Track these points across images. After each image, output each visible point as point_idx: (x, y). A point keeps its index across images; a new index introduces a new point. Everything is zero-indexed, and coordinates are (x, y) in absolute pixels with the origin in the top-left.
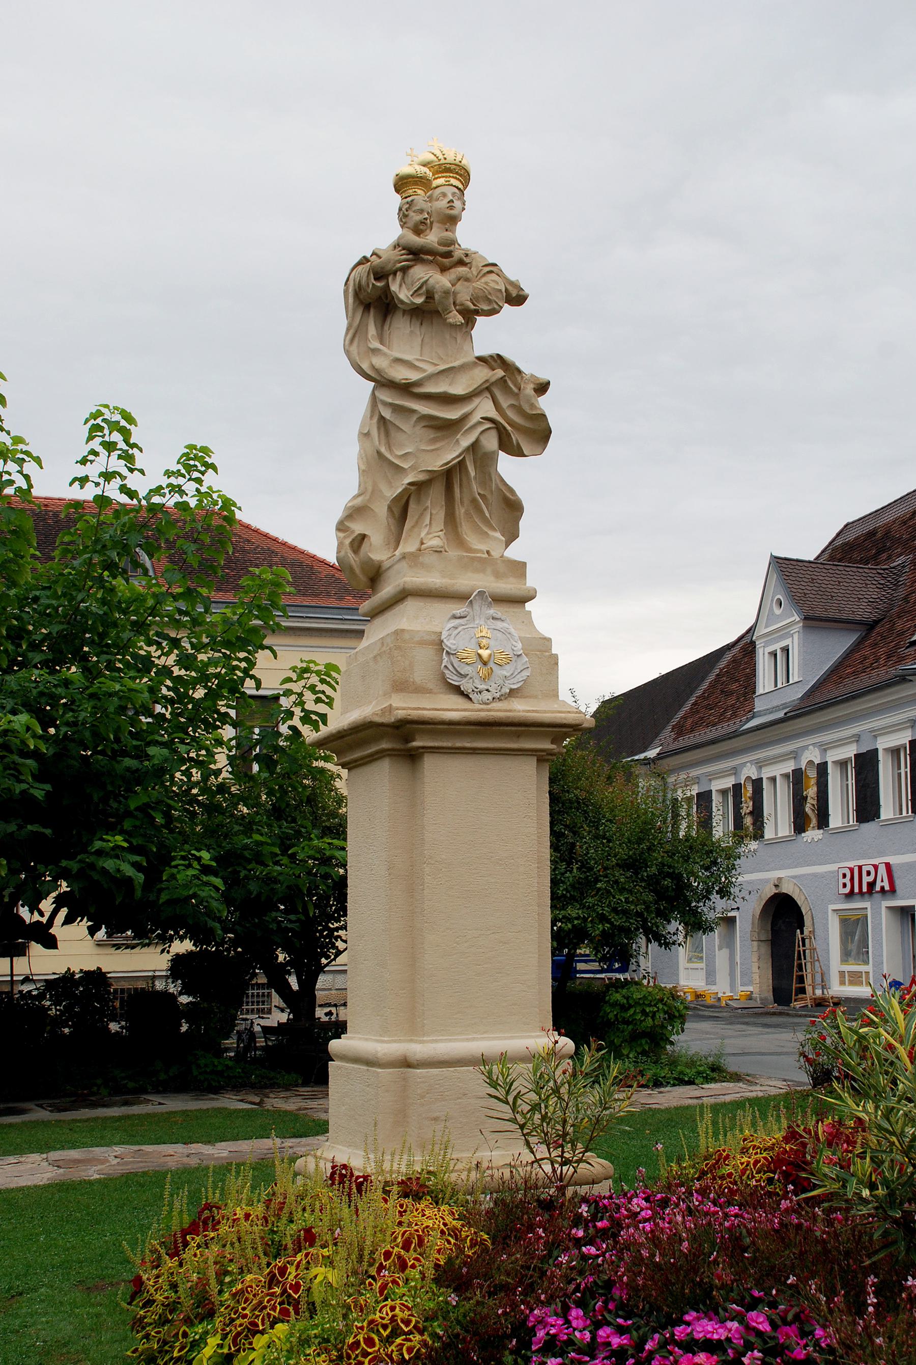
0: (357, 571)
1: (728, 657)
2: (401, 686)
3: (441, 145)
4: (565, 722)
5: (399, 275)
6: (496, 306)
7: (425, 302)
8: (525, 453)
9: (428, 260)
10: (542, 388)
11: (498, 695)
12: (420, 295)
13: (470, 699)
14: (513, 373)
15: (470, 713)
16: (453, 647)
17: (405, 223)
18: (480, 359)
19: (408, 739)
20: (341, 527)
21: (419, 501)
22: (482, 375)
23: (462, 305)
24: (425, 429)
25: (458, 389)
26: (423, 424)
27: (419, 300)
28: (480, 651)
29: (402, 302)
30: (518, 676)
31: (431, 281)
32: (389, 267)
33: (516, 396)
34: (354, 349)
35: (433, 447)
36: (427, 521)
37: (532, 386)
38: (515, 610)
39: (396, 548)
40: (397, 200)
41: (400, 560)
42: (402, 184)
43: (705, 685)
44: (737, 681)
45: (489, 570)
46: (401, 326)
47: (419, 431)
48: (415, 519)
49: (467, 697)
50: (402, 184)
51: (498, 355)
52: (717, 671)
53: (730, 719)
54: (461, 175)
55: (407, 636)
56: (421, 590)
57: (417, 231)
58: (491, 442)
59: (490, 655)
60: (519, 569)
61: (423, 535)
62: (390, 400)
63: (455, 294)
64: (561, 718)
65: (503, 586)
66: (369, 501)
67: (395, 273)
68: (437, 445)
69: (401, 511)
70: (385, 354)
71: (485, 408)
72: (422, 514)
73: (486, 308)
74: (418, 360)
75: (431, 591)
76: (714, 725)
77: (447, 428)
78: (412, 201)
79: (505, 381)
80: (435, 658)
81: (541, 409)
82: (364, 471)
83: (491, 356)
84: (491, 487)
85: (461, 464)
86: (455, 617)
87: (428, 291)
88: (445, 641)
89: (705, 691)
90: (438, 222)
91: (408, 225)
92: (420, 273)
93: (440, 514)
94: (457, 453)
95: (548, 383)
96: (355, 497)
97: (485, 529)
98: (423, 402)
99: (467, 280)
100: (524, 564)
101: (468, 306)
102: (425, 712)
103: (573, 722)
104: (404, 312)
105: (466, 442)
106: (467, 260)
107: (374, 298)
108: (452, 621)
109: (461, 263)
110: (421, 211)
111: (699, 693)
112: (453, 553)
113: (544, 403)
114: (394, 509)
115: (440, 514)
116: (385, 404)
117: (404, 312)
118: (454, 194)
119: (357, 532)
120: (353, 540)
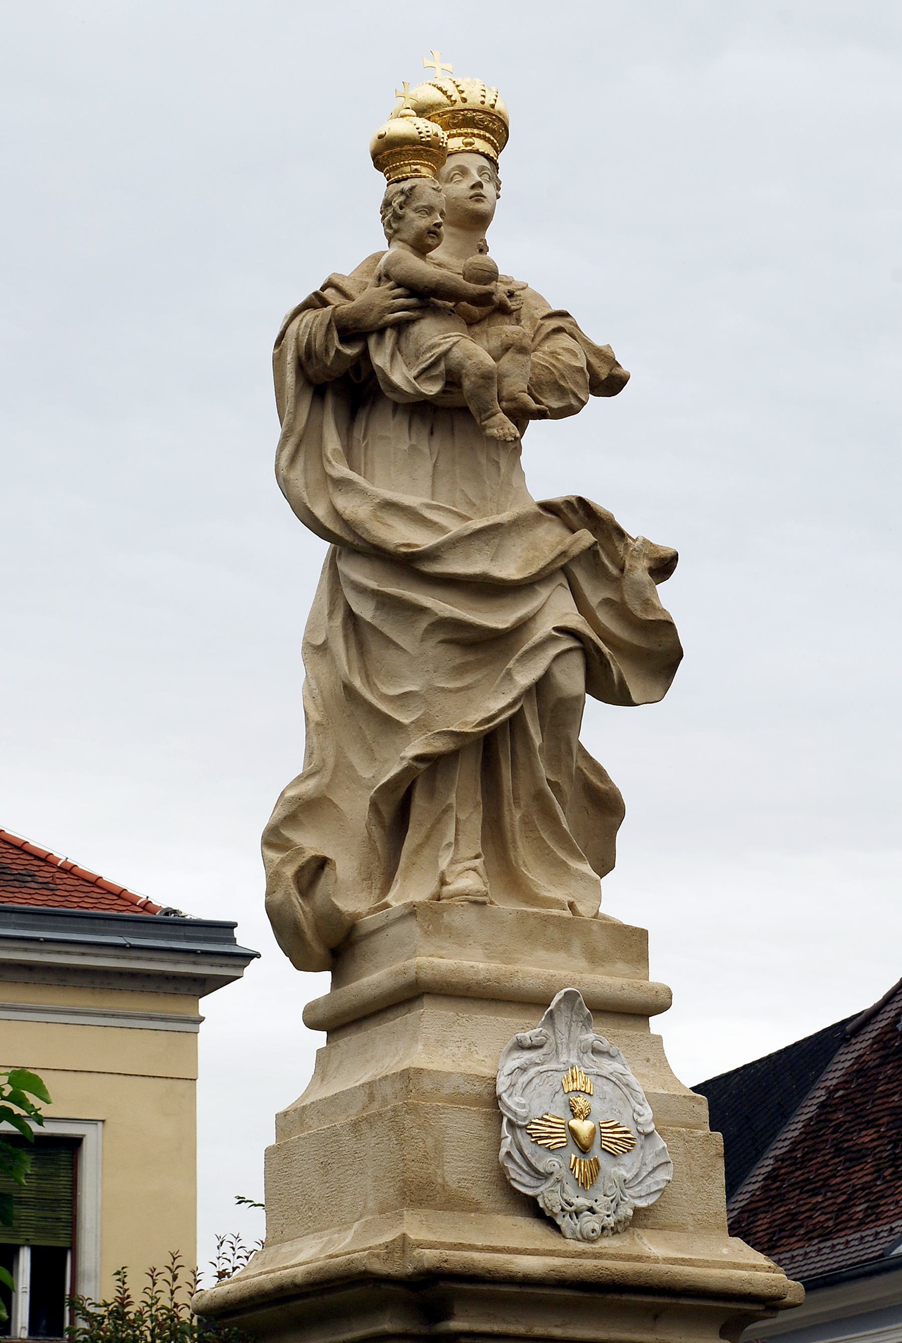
0: (309, 934)
1: (844, 1061)
2: (419, 1193)
3: (449, 66)
4: (749, 1289)
5: (390, 337)
6: (574, 402)
7: (443, 391)
8: (635, 698)
9: (445, 308)
10: (664, 567)
11: (611, 1221)
12: (433, 379)
13: (557, 1228)
14: (609, 538)
15: (569, 1261)
16: (521, 1111)
17: (396, 231)
18: (548, 507)
19: (439, 1310)
20: (273, 840)
21: (431, 793)
22: (551, 540)
23: (513, 399)
24: (443, 647)
25: (509, 569)
26: (442, 637)
27: (432, 389)
28: (575, 1123)
29: (395, 388)
30: (649, 1181)
31: (457, 353)
32: (371, 318)
33: (616, 582)
34: (297, 476)
36: (450, 837)
37: (645, 564)
38: (630, 1033)
39: (386, 889)
40: (377, 185)
41: (402, 918)
42: (389, 154)
43: (793, 1130)
44: (870, 1124)
45: (577, 946)
46: (390, 437)
47: (433, 649)
48: (424, 831)
49: (551, 1223)
50: (389, 154)
51: (580, 500)
52: (820, 1095)
53: (862, 1223)
54: (492, 132)
55: (427, 1084)
56: (449, 984)
57: (421, 247)
58: (571, 678)
59: (593, 1132)
60: (633, 943)
61: (443, 864)
62: (373, 584)
63: (501, 377)
64: (742, 1281)
65: (608, 980)
66: (328, 786)
67: (381, 332)
68: (468, 680)
69: (396, 812)
70: (363, 492)
71: (558, 609)
72: (438, 821)
73: (555, 404)
75: (468, 988)
76: (826, 1236)
77: (484, 647)
78: (412, 189)
79: (596, 554)
80: (485, 1134)
82: (318, 724)
83: (568, 503)
84: (569, 767)
85: (514, 725)
86: (520, 1046)
87: (449, 372)
88: (504, 1097)
89: (795, 1144)
90: (452, 224)
91: (405, 236)
92: (435, 335)
93: (474, 821)
94: (508, 699)
95: (675, 558)
96: (301, 779)
97: (562, 855)
98: (439, 592)
99: (523, 350)
100: (643, 934)
101: (525, 404)
102: (476, 1256)
103: (767, 1291)
104: (396, 406)
105: (525, 677)
106: (512, 304)
107: (336, 375)
108: (516, 1054)
109: (503, 310)
110: (429, 210)
111: (780, 1148)
112: (507, 907)
113: (670, 596)
114: (383, 808)
115: (473, 820)
117: (396, 406)
118: (481, 170)
119: (310, 853)
120: (301, 869)
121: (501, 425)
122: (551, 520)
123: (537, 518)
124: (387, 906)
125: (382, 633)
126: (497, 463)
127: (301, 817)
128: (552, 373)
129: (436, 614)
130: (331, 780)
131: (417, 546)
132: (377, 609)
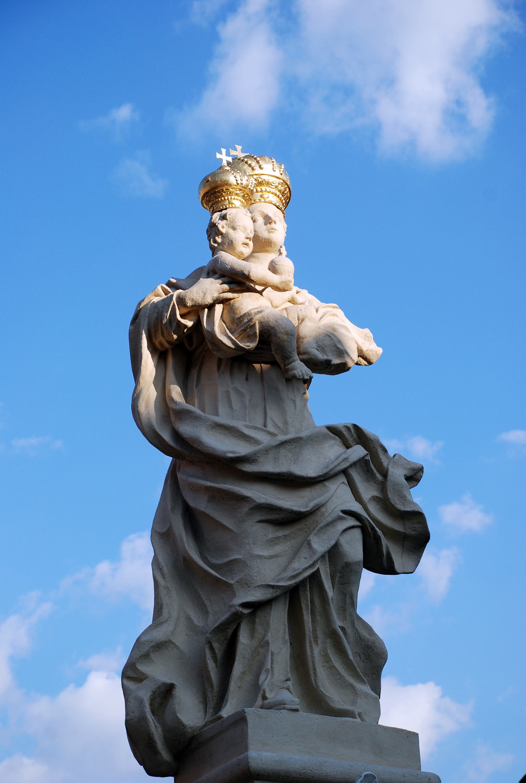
7: (257, 348)
8: (398, 566)
10: (414, 476)
18: (333, 430)
20: (131, 674)
22: (332, 453)
25: (308, 466)
26: (259, 518)
51: (355, 426)
58: (354, 548)
66: (173, 633)
74: (247, 427)
81: (413, 503)
85: (315, 577)
97: (350, 679)
105: (320, 545)
113: (419, 497)
114: (215, 645)
116: (196, 489)
121: (300, 368)
122: (334, 439)
123: (325, 437)
124: (220, 717)
125: (213, 519)
126: (294, 401)
127: (152, 655)
128: (332, 339)
129: (255, 501)
130: (175, 628)
131: (240, 453)
132: (209, 501)
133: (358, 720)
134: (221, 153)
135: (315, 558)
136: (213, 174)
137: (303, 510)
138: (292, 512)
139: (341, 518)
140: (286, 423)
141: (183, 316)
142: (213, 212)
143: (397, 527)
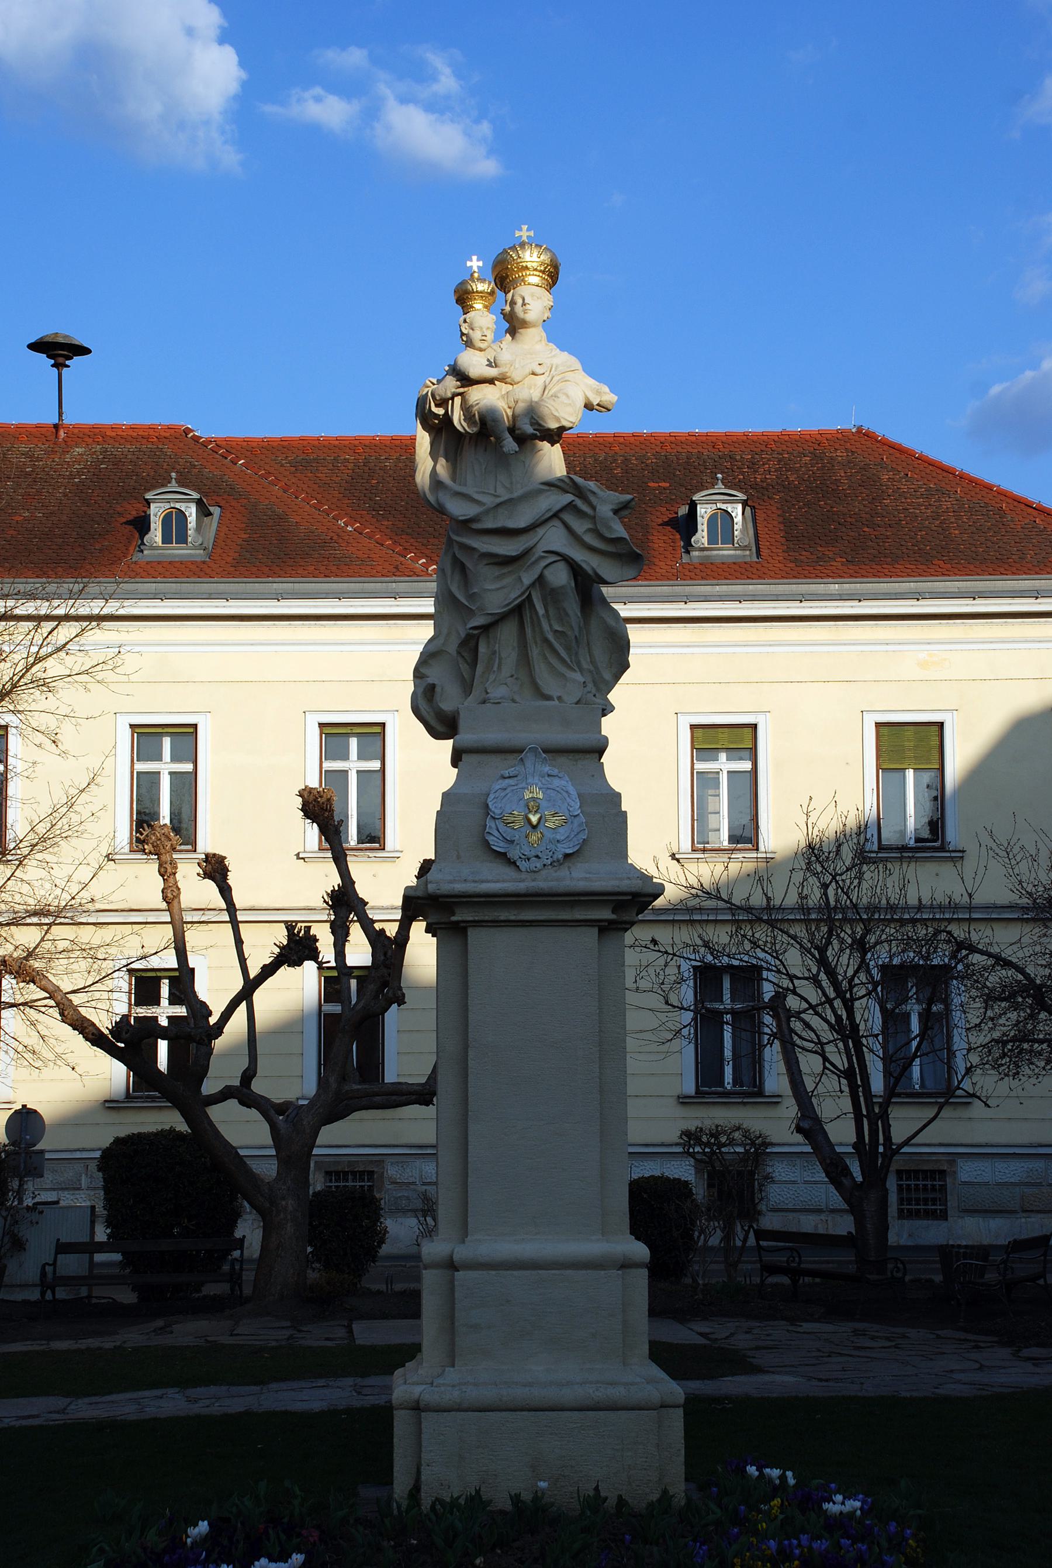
35: (498, 586)
74: (477, 492)
97: (562, 669)
105: (527, 579)
108: (500, 781)
114: (465, 654)
123: (540, 492)
133: (556, 702)
134: (528, 230)
135: (524, 588)
136: (464, 283)
137: (514, 554)
138: (506, 556)
139: (543, 557)
140: (511, 483)
141: (437, 406)
142: (506, 294)
143: (610, 548)
